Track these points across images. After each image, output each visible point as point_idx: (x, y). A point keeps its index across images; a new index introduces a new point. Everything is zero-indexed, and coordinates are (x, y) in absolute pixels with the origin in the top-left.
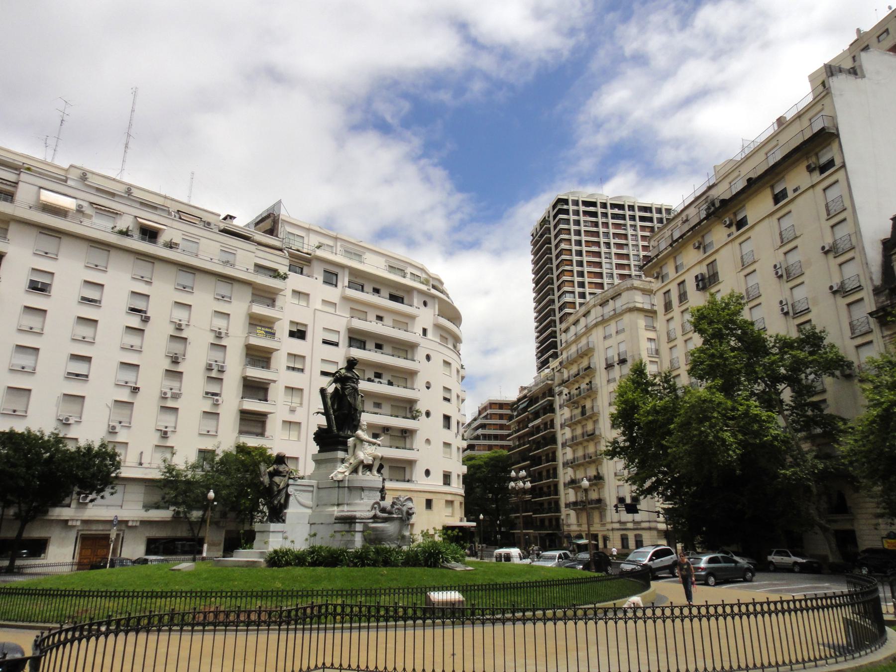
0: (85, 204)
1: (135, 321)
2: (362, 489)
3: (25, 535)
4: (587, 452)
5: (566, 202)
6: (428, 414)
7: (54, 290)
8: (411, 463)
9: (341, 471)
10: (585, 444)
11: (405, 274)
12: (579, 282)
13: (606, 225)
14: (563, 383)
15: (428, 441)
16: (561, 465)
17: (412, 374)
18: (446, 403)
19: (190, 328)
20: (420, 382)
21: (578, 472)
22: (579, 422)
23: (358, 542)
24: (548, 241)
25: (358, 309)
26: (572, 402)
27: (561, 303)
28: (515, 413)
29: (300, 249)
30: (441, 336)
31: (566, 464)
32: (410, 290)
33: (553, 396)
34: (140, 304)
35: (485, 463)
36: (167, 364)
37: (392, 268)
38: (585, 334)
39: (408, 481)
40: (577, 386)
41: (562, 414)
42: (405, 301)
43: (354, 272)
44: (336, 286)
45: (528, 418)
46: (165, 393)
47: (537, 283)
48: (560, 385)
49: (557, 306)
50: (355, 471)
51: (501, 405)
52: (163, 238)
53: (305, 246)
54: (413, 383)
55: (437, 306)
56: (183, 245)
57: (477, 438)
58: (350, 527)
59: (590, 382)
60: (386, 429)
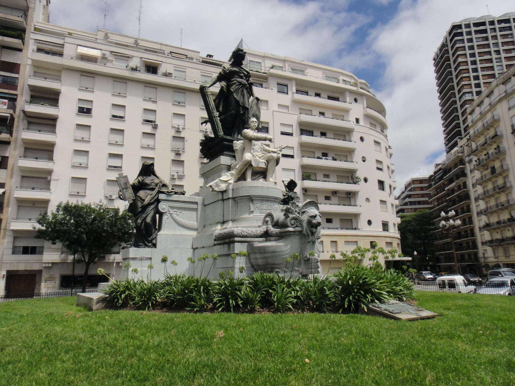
0: (108, 54)
1: (148, 129)
2: (251, 199)
3: (91, 272)
4: (499, 202)
5: (459, 26)
6: (366, 180)
7: (94, 112)
8: (356, 216)
9: (227, 179)
10: (497, 196)
11: (338, 80)
12: (475, 84)
13: (495, 37)
14: (473, 152)
15: (368, 200)
16: (475, 214)
17: (351, 151)
18: (379, 172)
19: (186, 130)
20: (357, 157)
21: (491, 218)
22: (490, 179)
23: (239, 269)
24: (448, 59)
25: (305, 108)
26: (481, 165)
27: (462, 101)
28: (433, 183)
29: (260, 71)
30: (370, 123)
31: (479, 213)
32: (343, 91)
33: (464, 164)
34: (150, 117)
35: (413, 219)
36: (172, 156)
37: (328, 78)
38: (489, 110)
39: (355, 229)
40: (485, 152)
41: (473, 176)
42: (340, 99)
43: (299, 83)
44: (287, 93)
45: (444, 184)
46: (173, 176)
47: (440, 92)
48: (469, 155)
49: (459, 104)
50: (242, 177)
51: (421, 181)
52: (162, 70)
53: (263, 68)
54: (352, 158)
55: (365, 102)
56: (174, 74)
57: (406, 204)
58: (229, 248)
59: (498, 147)
60: (335, 193)
